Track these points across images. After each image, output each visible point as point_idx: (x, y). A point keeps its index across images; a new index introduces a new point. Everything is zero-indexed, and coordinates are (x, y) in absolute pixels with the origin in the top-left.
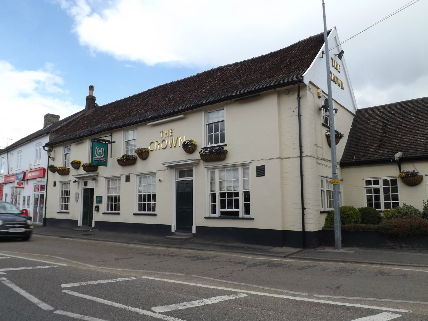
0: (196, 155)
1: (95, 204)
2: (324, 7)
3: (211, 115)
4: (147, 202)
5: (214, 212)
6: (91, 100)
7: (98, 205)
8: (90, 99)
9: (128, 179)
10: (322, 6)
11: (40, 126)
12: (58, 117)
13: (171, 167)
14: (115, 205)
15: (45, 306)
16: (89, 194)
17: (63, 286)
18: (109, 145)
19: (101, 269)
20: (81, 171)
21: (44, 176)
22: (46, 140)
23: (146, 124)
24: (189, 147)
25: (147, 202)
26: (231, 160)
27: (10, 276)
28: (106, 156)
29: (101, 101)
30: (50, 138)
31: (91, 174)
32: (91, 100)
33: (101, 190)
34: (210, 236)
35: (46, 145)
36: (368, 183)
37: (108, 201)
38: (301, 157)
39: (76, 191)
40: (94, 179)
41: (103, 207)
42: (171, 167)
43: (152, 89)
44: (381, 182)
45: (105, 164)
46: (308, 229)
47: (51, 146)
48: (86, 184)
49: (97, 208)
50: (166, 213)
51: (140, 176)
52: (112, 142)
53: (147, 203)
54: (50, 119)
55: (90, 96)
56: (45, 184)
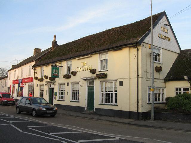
0: (95, 75)
1: (54, 96)
2: (151, 6)
3: (103, 56)
4: (76, 95)
5: (103, 102)
6: (55, 43)
7: (55, 96)
8: (54, 42)
9: (68, 85)
10: (150, 5)
11: (31, 54)
12: (40, 50)
13: (85, 80)
14: (76, 97)
15: (21, 131)
16: (52, 90)
17: (28, 127)
18: (60, 68)
19: (44, 123)
20: (48, 80)
21: (32, 81)
22: (33, 63)
23: (75, 59)
24: (93, 71)
25: (76, 95)
26: (109, 78)
27: (13, 123)
28: (58, 73)
29: (60, 43)
30: (35, 63)
31: (52, 82)
32: (55, 43)
33: (56, 89)
34: (100, 112)
35: (33, 67)
36: (177, 89)
37: (60, 94)
38: (138, 78)
39: (46, 89)
40: (53, 84)
41: (57, 97)
42: (85, 80)
43: (88, 36)
44: (182, 90)
45: (58, 77)
46: (140, 111)
47: (35, 67)
48: (50, 86)
49: (55, 98)
50: (83, 102)
51: (73, 84)
52: (61, 67)
53: (108, 98)
54: (37, 50)
55: (54, 41)
56: (33, 85)
